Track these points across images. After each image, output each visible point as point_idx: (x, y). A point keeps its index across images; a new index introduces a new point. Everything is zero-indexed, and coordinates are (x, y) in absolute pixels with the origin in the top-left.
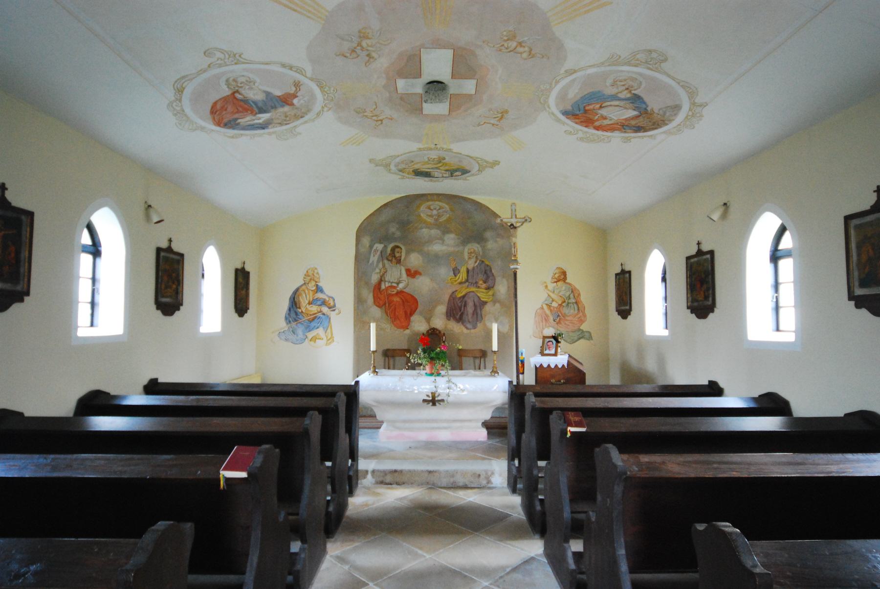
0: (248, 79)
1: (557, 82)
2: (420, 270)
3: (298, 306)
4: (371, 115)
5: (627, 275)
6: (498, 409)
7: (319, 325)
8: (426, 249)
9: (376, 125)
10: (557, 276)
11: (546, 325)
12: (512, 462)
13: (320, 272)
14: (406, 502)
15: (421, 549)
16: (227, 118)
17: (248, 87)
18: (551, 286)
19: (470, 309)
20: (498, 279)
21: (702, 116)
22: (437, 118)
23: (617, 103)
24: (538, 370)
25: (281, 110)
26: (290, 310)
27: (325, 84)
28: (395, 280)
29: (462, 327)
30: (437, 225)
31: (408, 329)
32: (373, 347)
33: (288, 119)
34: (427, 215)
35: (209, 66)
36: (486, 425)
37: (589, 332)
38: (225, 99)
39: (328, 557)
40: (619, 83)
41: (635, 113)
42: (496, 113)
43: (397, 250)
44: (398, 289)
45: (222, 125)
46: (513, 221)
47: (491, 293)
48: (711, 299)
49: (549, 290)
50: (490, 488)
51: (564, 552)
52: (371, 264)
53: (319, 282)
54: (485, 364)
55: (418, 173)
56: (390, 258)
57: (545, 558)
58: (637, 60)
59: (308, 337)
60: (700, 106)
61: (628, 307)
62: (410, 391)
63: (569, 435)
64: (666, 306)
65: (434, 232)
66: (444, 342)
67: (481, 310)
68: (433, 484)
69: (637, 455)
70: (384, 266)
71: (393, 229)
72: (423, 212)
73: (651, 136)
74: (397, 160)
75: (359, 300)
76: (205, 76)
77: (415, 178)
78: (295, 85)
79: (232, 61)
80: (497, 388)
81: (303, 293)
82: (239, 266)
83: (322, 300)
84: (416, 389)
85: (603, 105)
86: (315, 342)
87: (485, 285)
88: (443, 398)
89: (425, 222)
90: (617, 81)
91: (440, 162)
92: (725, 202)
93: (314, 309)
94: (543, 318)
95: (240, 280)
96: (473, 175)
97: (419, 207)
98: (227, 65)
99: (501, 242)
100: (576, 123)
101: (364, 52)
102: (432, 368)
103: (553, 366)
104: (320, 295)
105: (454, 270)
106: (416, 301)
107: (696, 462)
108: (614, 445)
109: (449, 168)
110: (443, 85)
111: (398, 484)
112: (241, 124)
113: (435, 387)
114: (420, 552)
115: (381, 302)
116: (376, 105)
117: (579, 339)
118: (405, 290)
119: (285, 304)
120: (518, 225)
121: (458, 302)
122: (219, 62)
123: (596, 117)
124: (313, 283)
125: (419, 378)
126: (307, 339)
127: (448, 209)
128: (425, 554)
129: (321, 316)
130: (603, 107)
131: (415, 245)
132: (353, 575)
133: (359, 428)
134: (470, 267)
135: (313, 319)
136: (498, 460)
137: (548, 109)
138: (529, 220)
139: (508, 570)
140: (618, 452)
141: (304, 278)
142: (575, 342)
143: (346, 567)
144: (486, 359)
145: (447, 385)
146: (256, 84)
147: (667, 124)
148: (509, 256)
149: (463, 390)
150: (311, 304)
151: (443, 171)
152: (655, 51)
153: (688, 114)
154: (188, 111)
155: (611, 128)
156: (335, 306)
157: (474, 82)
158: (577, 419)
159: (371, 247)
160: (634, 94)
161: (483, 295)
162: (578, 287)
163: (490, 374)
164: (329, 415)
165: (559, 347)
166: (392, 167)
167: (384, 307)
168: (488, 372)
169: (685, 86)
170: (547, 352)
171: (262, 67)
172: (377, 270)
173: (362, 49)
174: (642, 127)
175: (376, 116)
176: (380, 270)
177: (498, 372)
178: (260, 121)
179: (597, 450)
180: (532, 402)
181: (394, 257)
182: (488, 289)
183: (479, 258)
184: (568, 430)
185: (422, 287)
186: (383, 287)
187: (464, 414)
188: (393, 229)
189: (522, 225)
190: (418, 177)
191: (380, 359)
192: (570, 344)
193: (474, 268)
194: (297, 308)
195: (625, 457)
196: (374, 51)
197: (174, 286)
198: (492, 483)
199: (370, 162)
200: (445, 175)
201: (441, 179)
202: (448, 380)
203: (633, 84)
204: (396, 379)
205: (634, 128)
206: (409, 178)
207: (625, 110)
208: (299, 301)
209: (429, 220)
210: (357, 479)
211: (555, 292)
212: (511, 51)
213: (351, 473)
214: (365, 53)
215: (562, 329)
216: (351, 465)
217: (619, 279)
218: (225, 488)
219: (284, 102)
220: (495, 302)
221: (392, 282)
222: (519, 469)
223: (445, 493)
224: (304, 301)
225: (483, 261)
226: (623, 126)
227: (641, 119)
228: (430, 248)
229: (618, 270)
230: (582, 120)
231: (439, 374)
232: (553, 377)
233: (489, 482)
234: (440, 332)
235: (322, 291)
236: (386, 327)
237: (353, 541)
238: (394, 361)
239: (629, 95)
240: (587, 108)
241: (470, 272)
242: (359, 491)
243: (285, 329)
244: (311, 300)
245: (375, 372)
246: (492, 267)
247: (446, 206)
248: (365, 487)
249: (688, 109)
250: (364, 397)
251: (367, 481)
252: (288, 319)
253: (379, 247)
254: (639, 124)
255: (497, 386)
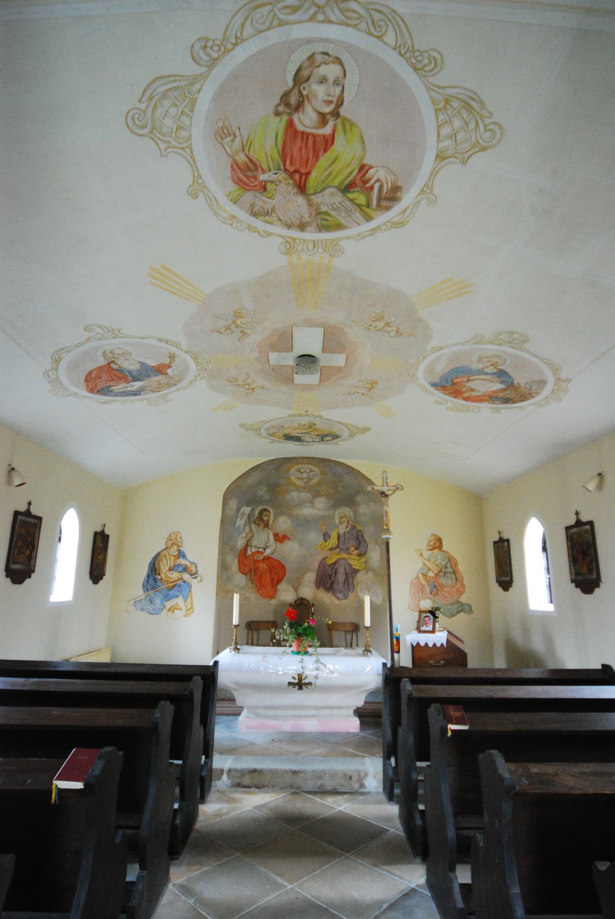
0: (124, 351)
1: (425, 358)
2: (289, 534)
3: (158, 573)
4: (242, 384)
5: (506, 543)
6: (372, 693)
7: (179, 593)
8: (295, 513)
9: (247, 393)
10: (432, 543)
11: (422, 597)
12: (388, 762)
13: (184, 537)
14: (265, 810)
15: (281, 875)
16: (101, 385)
17: (123, 358)
18: (427, 554)
19: (341, 578)
20: (370, 546)
21: (567, 390)
22: (307, 387)
23: (484, 377)
24: (415, 649)
25: (154, 379)
26: (148, 576)
27: (198, 355)
28: (261, 544)
29: (333, 597)
30: (307, 488)
31: (274, 598)
32: (235, 621)
33: (161, 387)
34: (297, 478)
35: (88, 340)
36: (360, 713)
37: (469, 605)
38: (100, 369)
39: (170, 886)
40: (484, 359)
41: (502, 386)
42: (365, 384)
43: (265, 513)
44: (265, 554)
45: (95, 392)
46: (384, 489)
47: (363, 560)
48: (595, 573)
49: (424, 559)
50: (363, 794)
51: (449, 882)
52: (237, 528)
53: (182, 547)
54: (357, 641)
55: (288, 437)
56: (258, 522)
57: (428, 890)
58: (501, 340)
59: (166, 606)
60: (565, 381)
61: (508, 579)
62: (274, 673)
63: (449, 734)
64: (549, 578)
65: (304, 495)
66: (313, 614)
67: (353, 579)
68: (298, 788)
69: (525, 764)
70: (251, 530)
71: (262, 492)
72: (293, 474)
73: (520, 407)
74: (268, 425)
75: (223, 567)
76: (83, 348)
77: (285, 442)
78: (169, 357)
79: (111, 335)
80: (370, 669)
81: (163, 558)
82: (99, 529)
83: (184, 567)
84: (281, 669)
85: (471, 378)
86: (173, 613)
87: (357, 551)
88: (310, 681)
89: (294, 485)
90: (482, 358)
91: (311, 427)
92: (600, 472)
93: (175, 575)
94: (420, 590)
95: (99, 544)
96: (344, 440)
97: (289, 470)
98: (106, 339)
99: (373, 506)
100: (445, 394)
101: (238, 329)
102: (299, 646)
103: (431, 645)
104: (182, 561)
105: (324, 535)
106: (283, 567)
107: (593, 774)
108: (500, 751)
109: (321, 433)
110: (313, 358)
111: (257, 787)
112: (114, 390)
113: (302, 668)
114: (280, 880)
115: (247, 570)
116: (248, 375)
117: (458, 612)
118: (272, 556)
119: (144, 570)
120: (390, 493)
121: (329, 569)
122: (98, 336)
123: (464, 389)
124: (175, 548)
125: (284, 657)
126: (164, 609)
127: (319, 472)
128: (285, 884)
129: (182, 583)
130: (471, 380)
131: (284, 509)
132: (199, 912)
133: (216, 714)
134: (342, 532)
135: (173, 587)
136: (372, 757)
137: (416, 381)
138: (401, 488)
139: (385, 906)
140: (504, 761)
141: (166, 542)
142: (454, 616)
143: (191, 901)
144: (359, 634)
145: (316, 665)
146: (132, 356)
147: (534, 397)
148: (380, 522)
149: (332, 672)
150: (172, 570)
151: (313, 436)
152: (517, 333)
153: (554, 388)
154: (63, 378)
155: (480, 399)
156: (197, 573)
157: (344, 356)
158: (458, 714)
159: (238, 509)
160: (500, 369)
161: (355, 563)
162: (455, 556)
163: (362, 653)
164: (182, 702)
165: (438, 622)
166: (263, 431)
167: (249, 575)
168: (360, 650)
169: (548, 364)
170: (424, 628)
171: (141, 341)
172: (244, 535)
173: (237, 326)
174: (510, 399)
175: (248, 385)
176: (247, 534)
177: (372, 650)
178: (133, 389)
179: (481, 756)
180: (408, 690)
181: (261, 521)
182: (361, 555)
183: (351, 522)
184: (449, 728)
185: (290, 552)
186: (249, 552)
187: (334, 699)
188: (262, 492)
189: (394, 493)
190: (288, 441)
191: (243, 632)
192: (450, 618)
193: (345, 534)
194: (156, 574)
195: (512, 766)
196: (247, 328)
197: (28, 552)
198: (366, 788)
199: (240, 427)
200: (315, 440)
201: (311, 443)
202: (316, 660)
203: (498, 361)
204: (259, 658)
205: (503, 400)
206: (279, 442)
207: (492, 384)
208: (159, 567)
209: (298, 483)
210: (211, 780)
211: (431, 561)
212: (379, 330)
213: (204, 774)
214: (239, 330)
215: (440, 602)
216: (205, 762)
217: (498, 547)
218: (57, 802)
219: (159, 372)
220: (368, 569)
221: (258, 548)
222: (395, 769)
223: (311, 799)
224: (164, 567)
225: (354, 527)
226: (491, 398)
227: (508, 391)
228: (300, 512)
229: (496, 538)
230: (451, 391)
231: (306, 653)
232: (430, 657)
233: (362, 786)
234: (308, 602)
235: (184, 556)
236: (251, 596)
237: (200, 864)
238: (259, 633)
239: (495, 370)
240: (455, 381)
241: (341, 537)
242: (212, 796)
243: (141, 598)
244: (172, 566)
245: (236, 649)
246: (364, 533)
247: (317, 469)
248: (219, 792)
249: (553, 384)
250: (223, 679)
251: (223, 783)
252: (145, 588)
253: (247, 510)
254: (507, 397)
255: (370, 667)
